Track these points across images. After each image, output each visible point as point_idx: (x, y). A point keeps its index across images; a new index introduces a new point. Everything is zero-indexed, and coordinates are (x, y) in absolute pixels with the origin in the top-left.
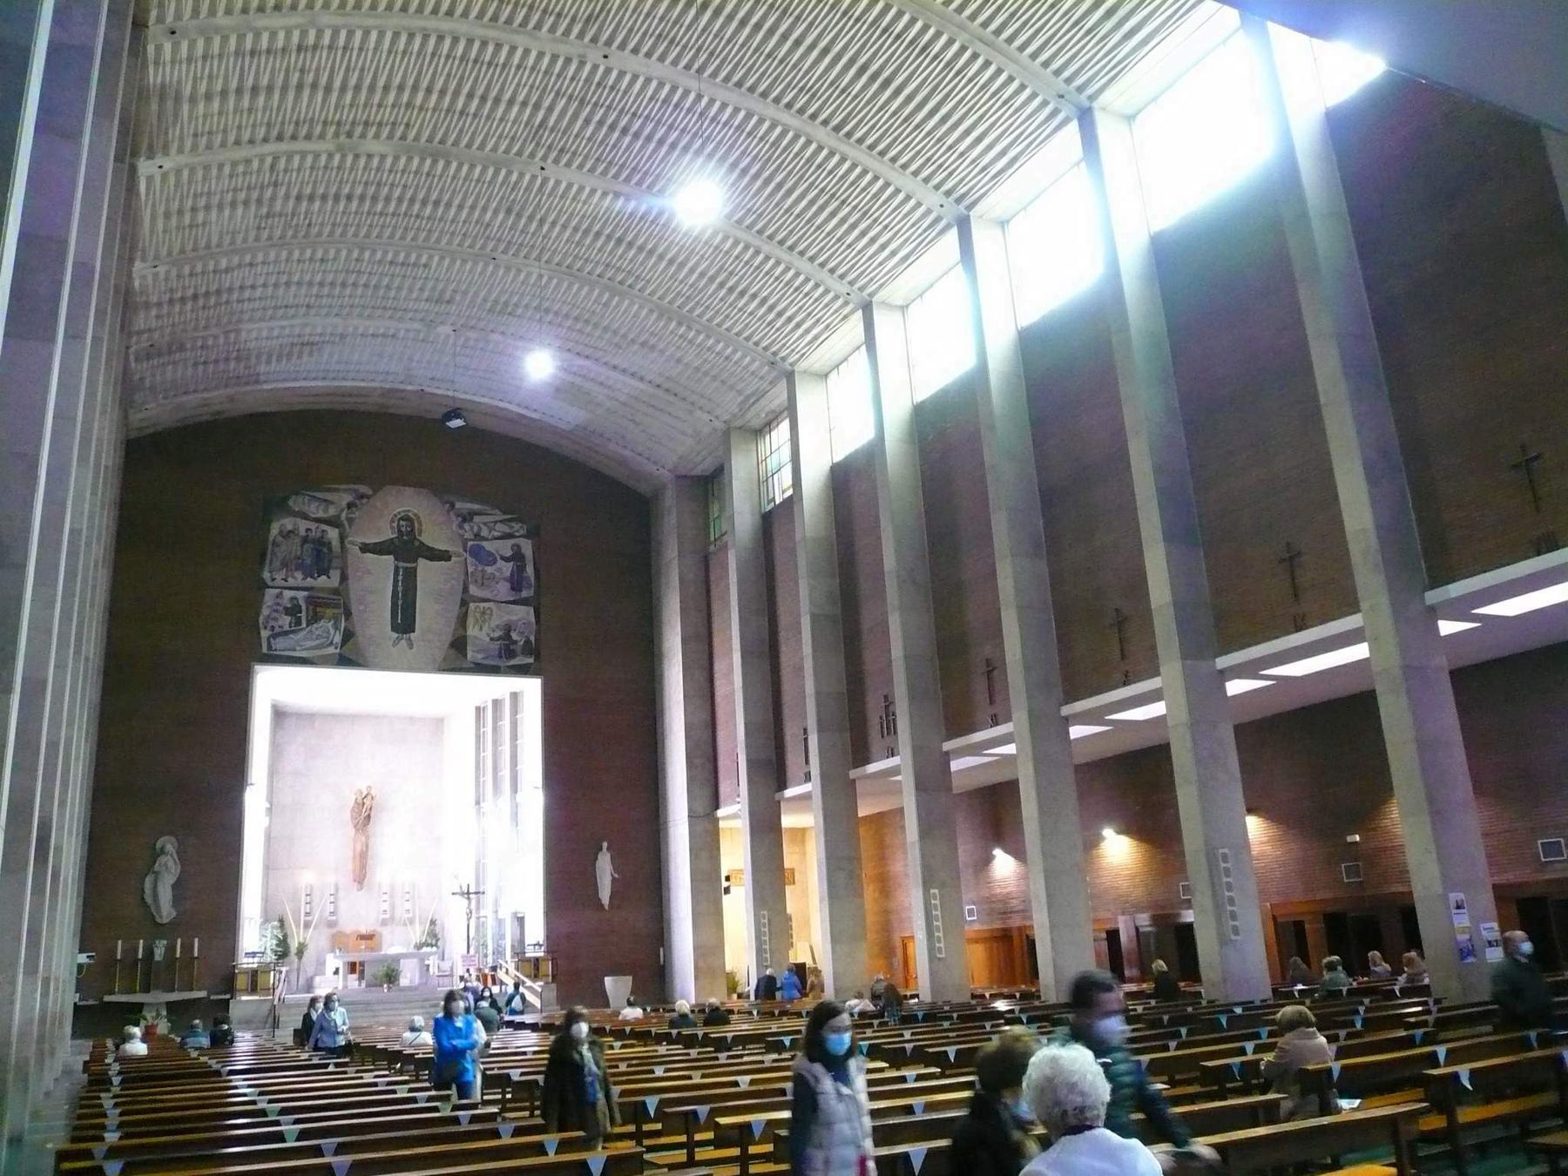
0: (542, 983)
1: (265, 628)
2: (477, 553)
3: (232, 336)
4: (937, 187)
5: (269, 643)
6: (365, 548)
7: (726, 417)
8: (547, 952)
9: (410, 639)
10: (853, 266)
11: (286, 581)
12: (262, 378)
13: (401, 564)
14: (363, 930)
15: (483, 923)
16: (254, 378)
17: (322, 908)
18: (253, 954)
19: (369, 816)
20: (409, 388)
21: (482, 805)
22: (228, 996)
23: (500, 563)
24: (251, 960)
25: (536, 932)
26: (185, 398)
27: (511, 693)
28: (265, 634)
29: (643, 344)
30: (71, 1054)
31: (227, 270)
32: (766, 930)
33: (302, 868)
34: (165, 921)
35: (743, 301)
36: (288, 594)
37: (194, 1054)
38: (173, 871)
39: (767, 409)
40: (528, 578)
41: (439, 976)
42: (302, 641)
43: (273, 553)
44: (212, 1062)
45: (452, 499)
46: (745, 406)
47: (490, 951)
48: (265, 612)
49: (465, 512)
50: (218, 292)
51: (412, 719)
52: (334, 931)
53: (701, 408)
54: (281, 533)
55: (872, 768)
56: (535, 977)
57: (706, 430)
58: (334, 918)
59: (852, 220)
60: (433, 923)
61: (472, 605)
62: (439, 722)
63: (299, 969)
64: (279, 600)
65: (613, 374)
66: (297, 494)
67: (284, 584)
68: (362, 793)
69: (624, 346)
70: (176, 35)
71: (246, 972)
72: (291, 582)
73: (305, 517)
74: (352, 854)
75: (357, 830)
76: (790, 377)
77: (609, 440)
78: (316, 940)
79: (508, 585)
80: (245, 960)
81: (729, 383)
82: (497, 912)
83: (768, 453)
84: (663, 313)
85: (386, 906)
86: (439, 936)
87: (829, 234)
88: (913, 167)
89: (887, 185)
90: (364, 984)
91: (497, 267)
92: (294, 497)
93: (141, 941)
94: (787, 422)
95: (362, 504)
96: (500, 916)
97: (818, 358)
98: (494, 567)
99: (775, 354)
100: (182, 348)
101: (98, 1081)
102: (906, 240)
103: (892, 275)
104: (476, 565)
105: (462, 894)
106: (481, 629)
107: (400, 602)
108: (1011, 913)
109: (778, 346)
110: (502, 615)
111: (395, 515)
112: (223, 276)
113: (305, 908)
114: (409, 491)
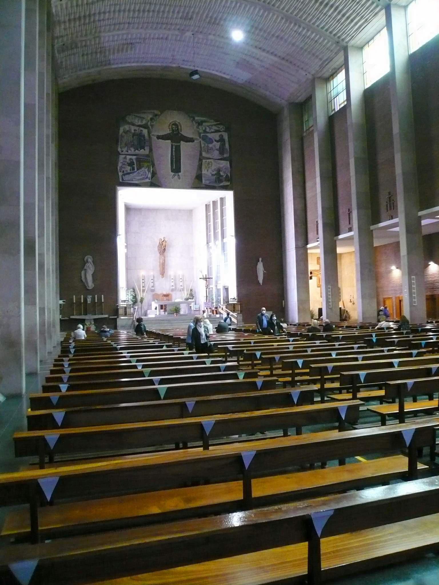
0: (236, 314)
1: (121, 171)
2: (205, 138)
3: (97, 39)
5: (122, 177)
6: (159, 137)
7: (313, 72)
8: (238, 301)
9: (179, 175)
11: (128, 152)
12: (112, 62)
13: (174, 144)
14: (165, 293)
15: (211, 290)
16: (108, 62)
17: (149, 284)
18: (125, 301)
19: (165, 249)
20: (174, 65)
21: (209, 244)
22: (116, 317)
23: (215, 143)
24: (123, 303)
25: (233, 294)
26: (79, 73)
27: (220, 198)
28: (120, 174)
29: (277, 37)
30: (58, 336)
32: (330, 293)
33: (140, 269)
34: (90, 288)
35: (327, 9)
36: (128, 157)
37: (105, 339)
39: (333, 67)
40: (227, 149)
41: (195, 311)
42: (135, 177)
44: (113, 343)
46: (322, 67)
47: (214, 301)
48: (120, 165)
50: (90, 15)
51: (180, 211)
52: (154, 293)
54: (124, 132)
55: (381, 225)
56: (234, 311)
58: (153, 288)
60: (191, 290)
61: (204, 161)
63: (141, 308)
64: (125, 160)
65: (264, 54)
66: (130, 115)
67: (126, 153)
68: (162, 240)
71: (122, 308)
73: (133, 125)
74: (159, 263)
75: (160, 254)
76: (345, 49)
78: (147, 297)
79: (218, 152)
80: (121, 303)
81: (316, 55)
82: (217, 286)
83: (332, 89)
85: (173, 284)
86: (194, 295)
90: (166, 313)
94: (344, 71)
96: (218, 288)
97: (359, 39)
99: (339, 37)
100: (76, 47)
101: (65, 351)
105: (204, 279)
106: (208, 171)
108: (435, 288)
109: (340, 33)
110: (215, 165)
111: (170, 123)
112: (91, 6)
113: (142, 284)
114: (175, 112)
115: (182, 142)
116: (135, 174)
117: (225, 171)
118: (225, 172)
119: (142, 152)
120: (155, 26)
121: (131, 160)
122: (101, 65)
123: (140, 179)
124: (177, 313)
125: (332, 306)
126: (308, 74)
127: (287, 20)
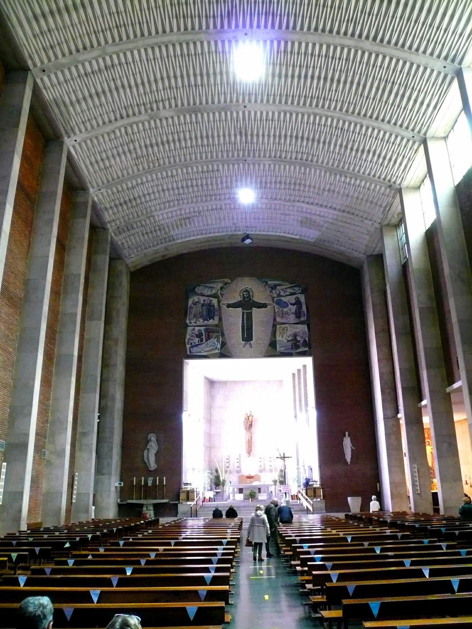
1: (188, 344)
2: (279, 303)
4: (439, 56)
5: (190, 350)
6: (229, 306)
7: (379, 221)
9: (250, 344)
10: (410, 119)
12: (175, 237)
17: (234, 465)
19: (251, 425)
20: (239, 233)
23: (290, 306)
25: (316, 477)
28: (188, 346)
31: (133, 187)
34: (152, 469)
36: (197, 329)
38: (155, 448)
42: (204, 349)
43: (190, 312)
45: (266, 280)
48: (188, 337)
49: (273, 285)
52: (240, 474)
53: (366, 218)
57: (373, 229)
58: (239, 469)
59: (401, 93)
61: (278, 327)
62: (281, 382)
64: (193, 332)
65: (323, 209)
66: (199, 286)
67: (195, 324)
68: (247, 414)
69: (321, 193)
70: (46, 72)
72: (198, 323)
73: (203, 295)
76: (400, 191)
77: (333, 243)
84: (331, 171)
87: (392, 105)
88: (422, 49)
89: (412, 64)
91: (249, 164)
92: (198, 287)
93: (143, 478)
95: (227, 287)
98: (288, 308)
99: (389, 181)
102: (433, 95)
103: (432, 119)
104: (279, 308)
105: (281, 458)
107: (245, 328)
111: (241, 290)
114: (247, 279)
115: (254, 309)
116: (204, 345)
117: (302, 335)
118: (302, 337)
119: (211, 322)
120: (209, 198)
121: (200, 332)
122: (166, 242)
123: (207, 351)
124: (252, 498)
125: (420, 491)
126: (374, 223)
127: (331, 173)
